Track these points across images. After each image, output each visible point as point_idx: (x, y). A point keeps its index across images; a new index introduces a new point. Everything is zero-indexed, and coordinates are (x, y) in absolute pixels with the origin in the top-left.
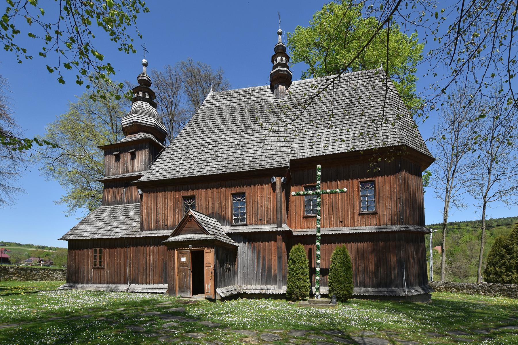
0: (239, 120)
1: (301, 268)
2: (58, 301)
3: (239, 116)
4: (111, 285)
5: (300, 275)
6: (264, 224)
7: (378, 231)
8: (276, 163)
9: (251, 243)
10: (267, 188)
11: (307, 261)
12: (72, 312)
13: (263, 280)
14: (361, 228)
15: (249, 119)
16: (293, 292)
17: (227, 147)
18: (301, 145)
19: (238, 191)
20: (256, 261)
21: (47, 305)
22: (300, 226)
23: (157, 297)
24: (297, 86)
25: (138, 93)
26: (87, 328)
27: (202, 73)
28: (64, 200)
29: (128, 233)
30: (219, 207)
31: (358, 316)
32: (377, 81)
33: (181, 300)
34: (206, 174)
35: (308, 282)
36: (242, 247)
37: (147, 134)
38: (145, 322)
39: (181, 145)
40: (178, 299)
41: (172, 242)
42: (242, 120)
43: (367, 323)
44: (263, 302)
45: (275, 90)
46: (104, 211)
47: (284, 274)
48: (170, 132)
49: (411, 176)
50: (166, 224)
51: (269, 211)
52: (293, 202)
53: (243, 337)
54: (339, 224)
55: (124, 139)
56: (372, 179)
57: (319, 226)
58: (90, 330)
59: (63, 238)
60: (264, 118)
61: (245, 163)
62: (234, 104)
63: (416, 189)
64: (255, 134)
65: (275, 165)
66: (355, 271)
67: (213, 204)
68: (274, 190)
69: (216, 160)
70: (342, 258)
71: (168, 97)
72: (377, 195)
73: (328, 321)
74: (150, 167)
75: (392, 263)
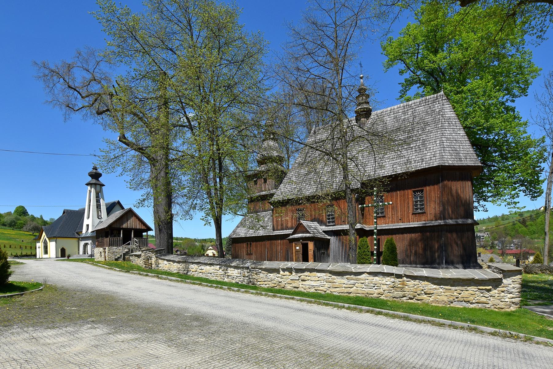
14: (414, 223)
20: (341, 248)
29: (266, 233)
36: (333, 239)
56: (421, 189)
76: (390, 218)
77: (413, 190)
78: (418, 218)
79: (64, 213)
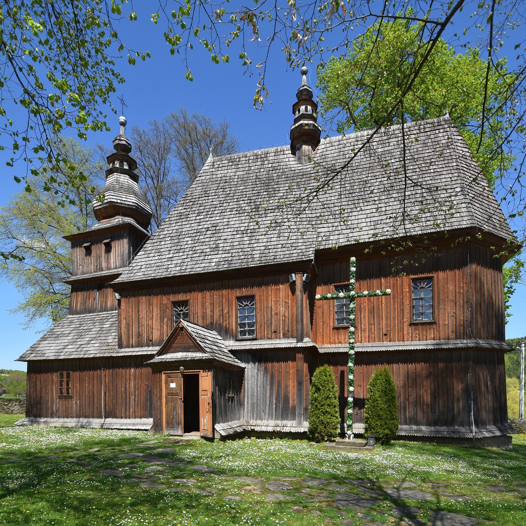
0: (248, 196)
1: (328, 397)
2: (17, 439)
3: (248, 190)
4: (81, 419)
5: (326, 407)
6: (280, 338)
8: (296, 255)
9: (263, 364)
10: (283, 288)
11: (337, 388)
12: (36, 453)
13: (277, 414)
15: (262, 194)
16: (317, 430)
17: (231, 233)
18: (331, 229)
19: (244, 294)
20: (268, 387)
21: (4, 444)
22: (328, 341)
23: (140, 435)
24: (328, 145)
25: (114, 163)
26: (55, 471)
27: (199, 128)
28: (20, 308)
29: (103, 351)
30: (220, 315)
31: (400, 464)
32: (440, 135)
33: (170, 439)
34: (202, 272)
35: (337, 417)
37: (126, 218)
38: (123, 465)
39: (171, 232)
40: (166, 437)
41: (158, 363)
42: (251, 195)
43: (410, 473)
44: (277, 442)
45: (297, 152)
46: (71, 322)
47: (306, 405)
48: (157, 211)
49: (485, 270)
50: (151, 339)
51: (287, 320)
52: (320, 307)
53: (244, 485)
54: (383, 338)
55: (97, 226)
56: (429, 275)
57: (352, 341)
58: (59, 473)
59: (21, 359)
60: (281, 192)
61: (255, 256)
62: (241, 173)
63: (493, 288)
64: (269, 215)
65: (294, 258)
66: (404, 402)
67: (212, 311)
68: (293, 291)
69: (216, 252)
70: (383, 384)
71: (153, 164)
72: (436, 298)
73: (357, 468)
74: (130, 263)
75: (455, 393)
77: (413, 277)
78: (421, 333)
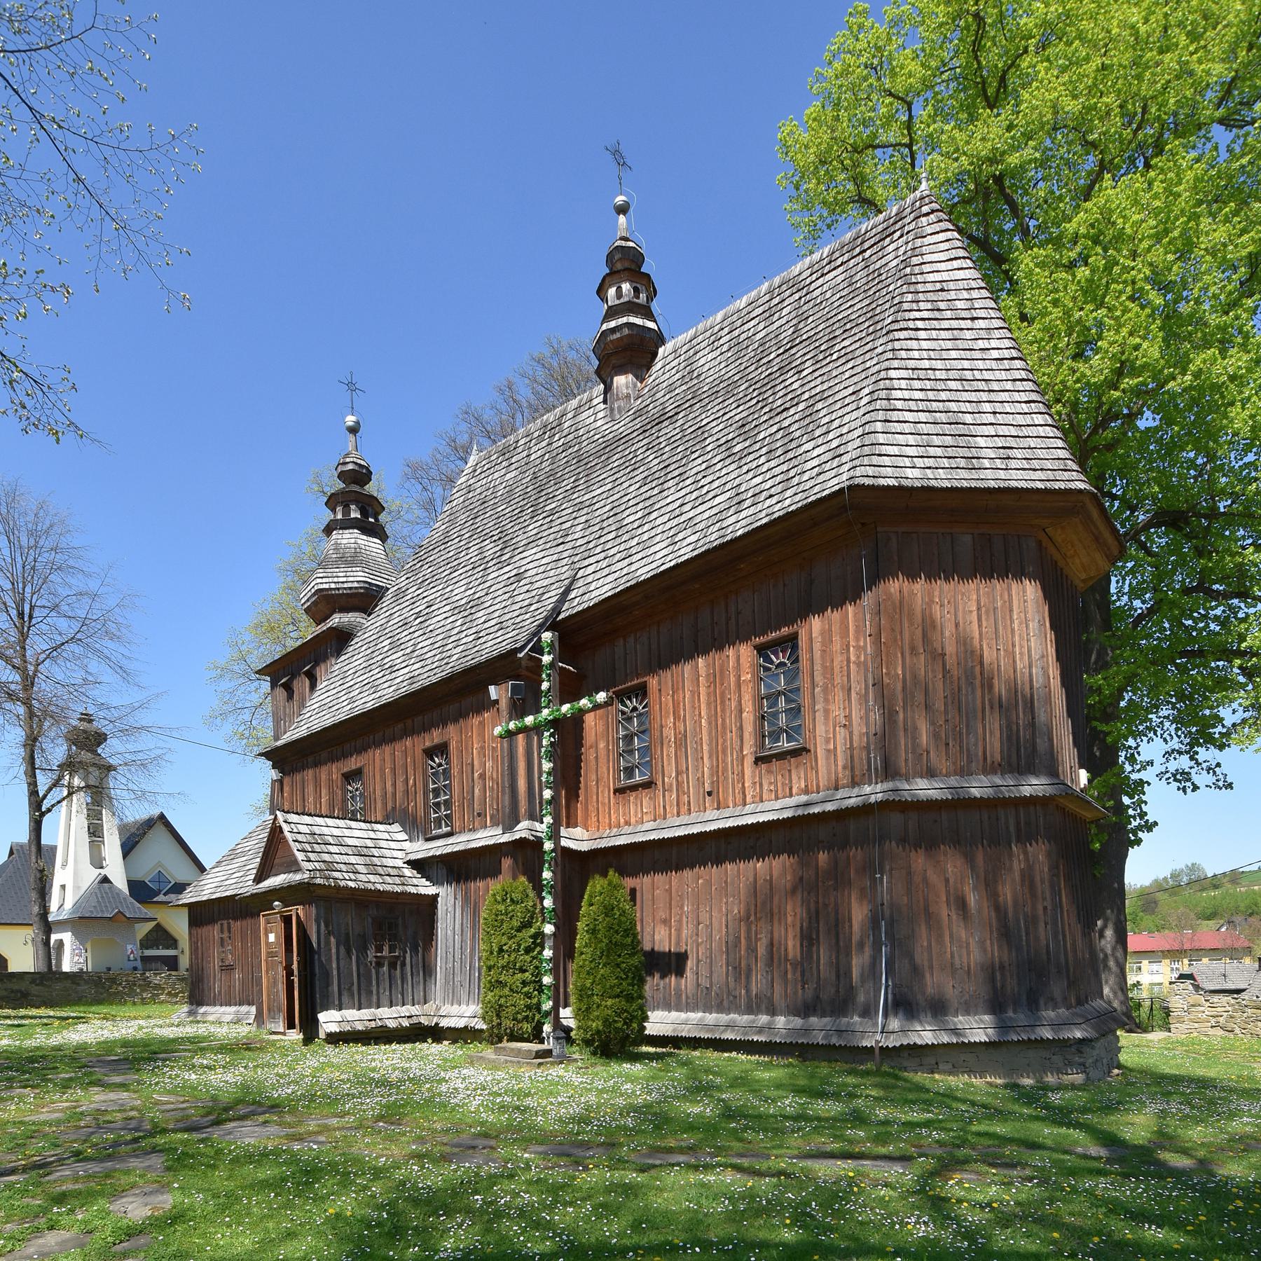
7: (800, 812)
14: (761, 807)
36: (446, 896)
52: (591, 747)
67: (394, 785)
76: (670, 790)
79: (11, 853)
